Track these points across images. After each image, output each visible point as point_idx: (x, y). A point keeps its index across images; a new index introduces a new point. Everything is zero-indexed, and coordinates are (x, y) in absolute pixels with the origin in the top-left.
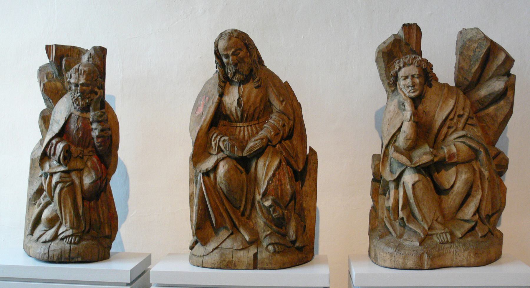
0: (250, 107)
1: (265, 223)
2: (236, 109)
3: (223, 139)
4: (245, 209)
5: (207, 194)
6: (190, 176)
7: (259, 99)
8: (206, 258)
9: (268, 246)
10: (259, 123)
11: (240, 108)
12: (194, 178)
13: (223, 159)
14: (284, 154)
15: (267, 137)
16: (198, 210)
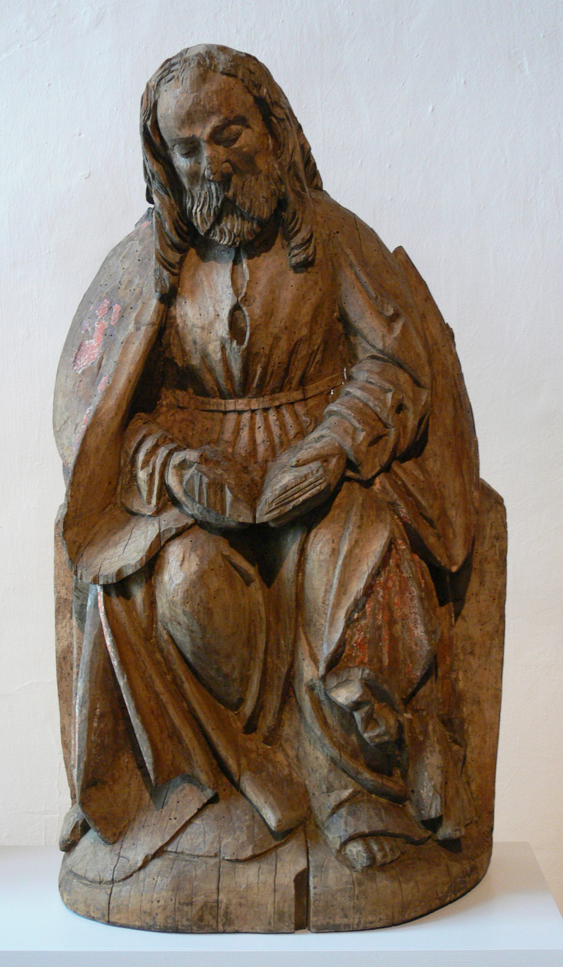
0: (277, 338)
1: (333, 761)
2: (223, 348)
3: (177, 459)
4: (259, 707)
5: (123, 662)
6: (57, 592)
7: (307, 310)
8: (124, 892)
9: (344, 844)
10: (305, 399)
11: (240, 343)
12: (72, 598)
13: (180, 533)
14: (403, 511)
15: (341, 452)
16: (90, 718)
